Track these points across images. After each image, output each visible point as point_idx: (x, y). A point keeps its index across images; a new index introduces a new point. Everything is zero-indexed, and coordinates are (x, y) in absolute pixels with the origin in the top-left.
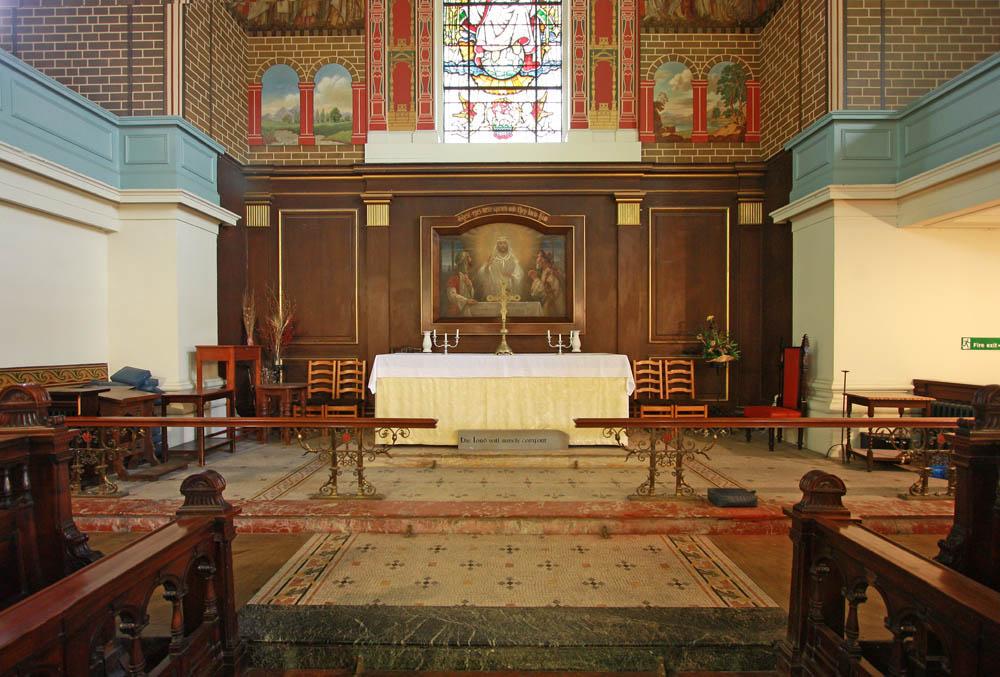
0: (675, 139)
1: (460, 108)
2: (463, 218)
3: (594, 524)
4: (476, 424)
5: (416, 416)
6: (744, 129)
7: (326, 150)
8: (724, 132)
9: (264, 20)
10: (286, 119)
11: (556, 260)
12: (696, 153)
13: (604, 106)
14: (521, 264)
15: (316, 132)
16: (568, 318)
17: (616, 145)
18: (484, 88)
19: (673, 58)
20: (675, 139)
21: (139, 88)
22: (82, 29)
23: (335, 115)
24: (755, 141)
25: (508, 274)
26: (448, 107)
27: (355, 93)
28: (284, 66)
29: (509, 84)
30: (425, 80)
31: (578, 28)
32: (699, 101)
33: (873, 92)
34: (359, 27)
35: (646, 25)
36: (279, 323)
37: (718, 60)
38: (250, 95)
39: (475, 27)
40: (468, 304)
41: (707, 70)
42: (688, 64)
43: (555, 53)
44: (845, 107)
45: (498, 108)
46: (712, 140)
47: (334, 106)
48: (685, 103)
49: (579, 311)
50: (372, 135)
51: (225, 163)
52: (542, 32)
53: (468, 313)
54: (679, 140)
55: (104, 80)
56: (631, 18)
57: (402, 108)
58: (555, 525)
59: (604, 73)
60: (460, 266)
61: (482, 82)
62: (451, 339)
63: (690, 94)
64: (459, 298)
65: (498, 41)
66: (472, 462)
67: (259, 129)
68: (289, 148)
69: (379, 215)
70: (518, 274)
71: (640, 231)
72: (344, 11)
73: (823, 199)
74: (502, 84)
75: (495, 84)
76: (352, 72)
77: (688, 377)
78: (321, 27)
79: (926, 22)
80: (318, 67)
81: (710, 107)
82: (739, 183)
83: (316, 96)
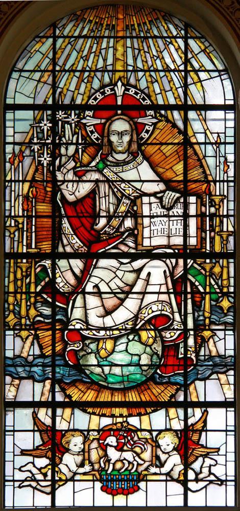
29: (133, 397)
39: (67, 297)
74: (118, 398)
75: (105, 397)
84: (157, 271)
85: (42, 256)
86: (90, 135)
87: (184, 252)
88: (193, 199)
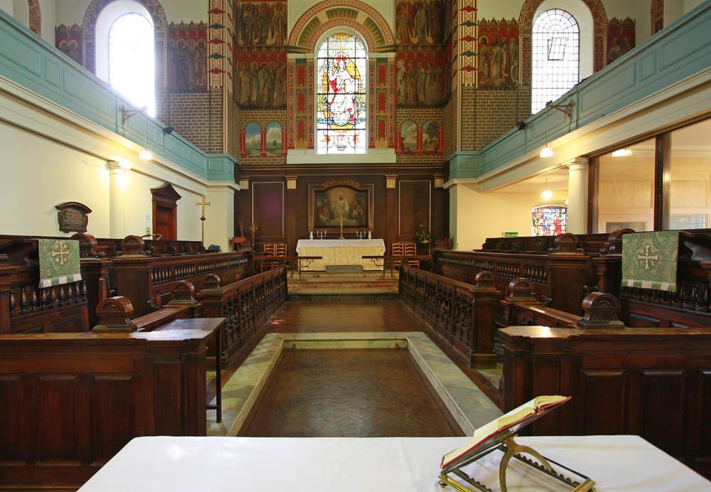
0: (409, 153)
1: (324, 138)
2: (325, 186)
3: (366, 284)
4: (332, 263)
5: (317, 256)
6: (437, 148)
7: (271, 159)
8: (429, 150)
9: (246, 104)
10: (256, 145)
11: (362, 202)
12: (418, 159)
13: (382, 139)
14: (349, 204)
15: (267, 150)
16: (367, 226)
17: (388, 156)
18: (334, 130)
19: (409, 120)
20: (409, 153)
21: (213, 143)
22: (197, 124)
23: (275, 143)
24: (441, 154)
25: (343, 208)
26: (320, 136)
27: (283, 134)
28: (254, 123)
29: (344, 128)
30: (310, 128)
31: (371, 107)
32: (419, 138)
33: (471, 144)
34: (284, 107)
35: (399, 106)
36: (253, 229)
37: (427, 120)
38: (241, 134)
39: (330, 104)
40: (327, 221)
41: (422, 124)
42: (415, 122)
43: (363, 115)
44: (461, 150)
45: (340, 138)
46: (424, 153)
47: (275, 139)
48: (413, 138)
49: (371, 224)
50: (290, 151)
51: (236, 166)
52: (358, 106)
53: (327, 224)
54: (411, 153)
55: (217, 149)
56: (393, 102)
57: (301, 140)
58: (355, 285)
59: (382, 125)
60: (324, 204)
61: (333, 127)
62: (323, 234)
63: (416, 134)
64: (324, 218)
65: (340, 110)
66: (331, 275)
67: (245, 149)
68: (256, 157)
69: (292, 185)
70: (347, 208)
71: (395, 190)
72: (278, 100)
73: (452, 184)
74: (341, 128)
75: (338, 128)
76: (282, 125)
77: (414, 250)
78: (269, 107)
79: (490, 118)
80: (268, 123)
81: (423, 140)
82: (435, 171)
83: (267, 135)
84: (350, 97)
85: (325, 94)
86: (605, 61)
87: (355, 93)
88: (246, 260)
